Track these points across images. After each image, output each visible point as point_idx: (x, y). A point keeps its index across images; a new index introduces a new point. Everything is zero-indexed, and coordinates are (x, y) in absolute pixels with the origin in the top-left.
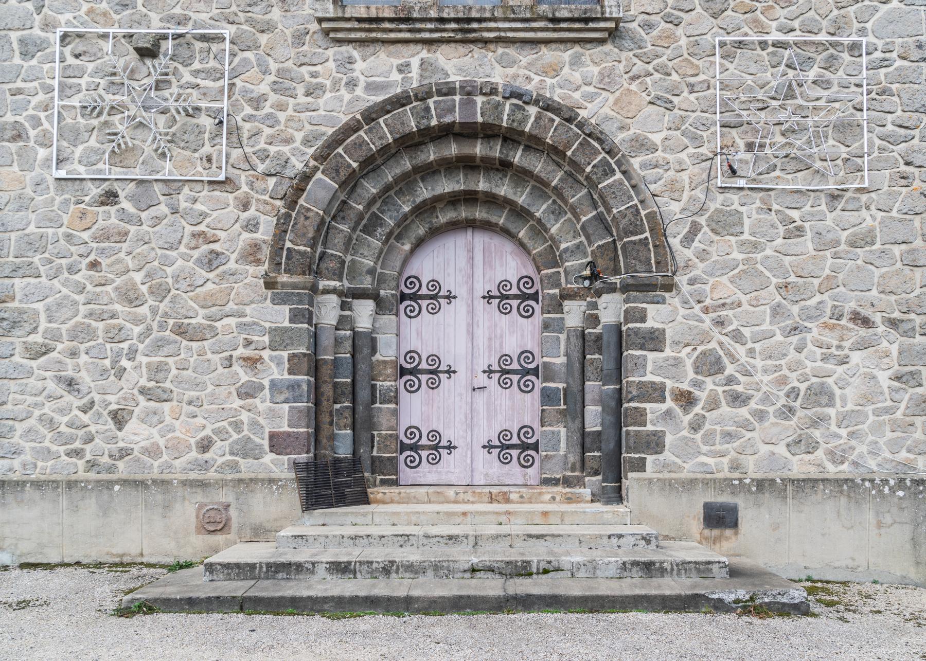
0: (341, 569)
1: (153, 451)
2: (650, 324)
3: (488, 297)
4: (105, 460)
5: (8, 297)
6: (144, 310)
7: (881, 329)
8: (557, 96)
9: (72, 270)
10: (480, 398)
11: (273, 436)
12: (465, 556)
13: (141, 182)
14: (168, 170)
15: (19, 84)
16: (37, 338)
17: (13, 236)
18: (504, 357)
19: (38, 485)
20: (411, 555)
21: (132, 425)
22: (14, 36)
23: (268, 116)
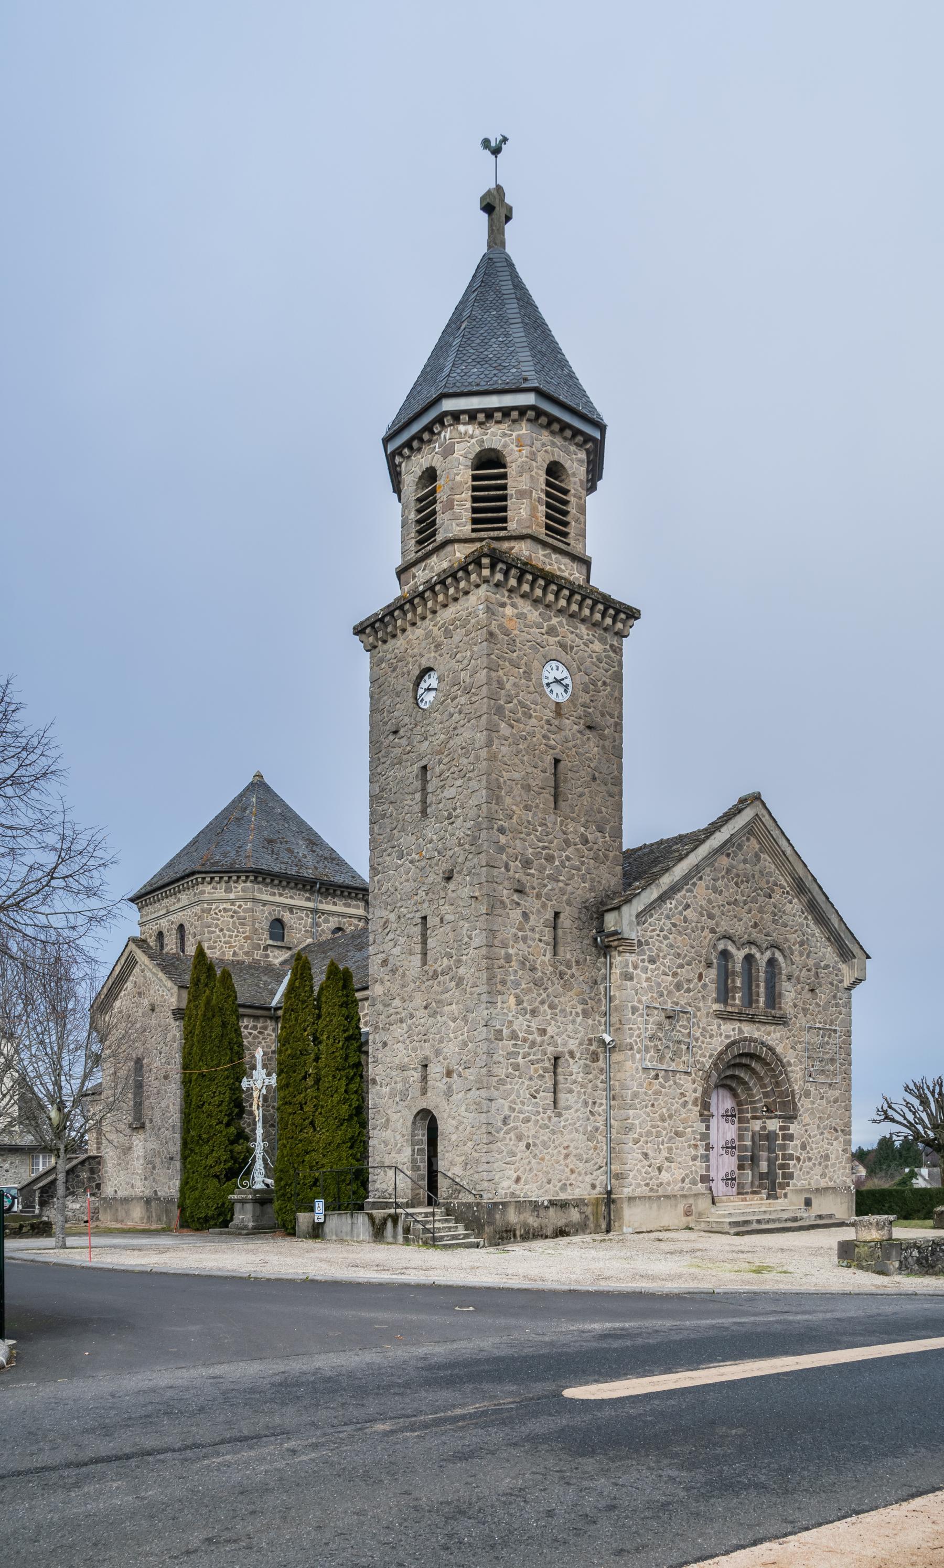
0: (759, 1221)
1: (669, 1184)
2: (791, 1131)
3: (723, 1116)
4: (655, 1187)
5: (844, 1151)
6: (666, 1124)
7: (840, 1133)
8: (770, 1043)
9: (646, 1107)
10: (720, 1159)
11: (701, 1176)
12: (785, 1216)
13: (666, 1071)
14: (673, 1066)
15: (631, 1026)
16: (636, 1136)
17: (630, 1092)
18: (727, 1142)
19: (640, 1198)
20: (767, 1217)
21: (663, 1172)
22: (630, 1004)
23: (700, 1046)
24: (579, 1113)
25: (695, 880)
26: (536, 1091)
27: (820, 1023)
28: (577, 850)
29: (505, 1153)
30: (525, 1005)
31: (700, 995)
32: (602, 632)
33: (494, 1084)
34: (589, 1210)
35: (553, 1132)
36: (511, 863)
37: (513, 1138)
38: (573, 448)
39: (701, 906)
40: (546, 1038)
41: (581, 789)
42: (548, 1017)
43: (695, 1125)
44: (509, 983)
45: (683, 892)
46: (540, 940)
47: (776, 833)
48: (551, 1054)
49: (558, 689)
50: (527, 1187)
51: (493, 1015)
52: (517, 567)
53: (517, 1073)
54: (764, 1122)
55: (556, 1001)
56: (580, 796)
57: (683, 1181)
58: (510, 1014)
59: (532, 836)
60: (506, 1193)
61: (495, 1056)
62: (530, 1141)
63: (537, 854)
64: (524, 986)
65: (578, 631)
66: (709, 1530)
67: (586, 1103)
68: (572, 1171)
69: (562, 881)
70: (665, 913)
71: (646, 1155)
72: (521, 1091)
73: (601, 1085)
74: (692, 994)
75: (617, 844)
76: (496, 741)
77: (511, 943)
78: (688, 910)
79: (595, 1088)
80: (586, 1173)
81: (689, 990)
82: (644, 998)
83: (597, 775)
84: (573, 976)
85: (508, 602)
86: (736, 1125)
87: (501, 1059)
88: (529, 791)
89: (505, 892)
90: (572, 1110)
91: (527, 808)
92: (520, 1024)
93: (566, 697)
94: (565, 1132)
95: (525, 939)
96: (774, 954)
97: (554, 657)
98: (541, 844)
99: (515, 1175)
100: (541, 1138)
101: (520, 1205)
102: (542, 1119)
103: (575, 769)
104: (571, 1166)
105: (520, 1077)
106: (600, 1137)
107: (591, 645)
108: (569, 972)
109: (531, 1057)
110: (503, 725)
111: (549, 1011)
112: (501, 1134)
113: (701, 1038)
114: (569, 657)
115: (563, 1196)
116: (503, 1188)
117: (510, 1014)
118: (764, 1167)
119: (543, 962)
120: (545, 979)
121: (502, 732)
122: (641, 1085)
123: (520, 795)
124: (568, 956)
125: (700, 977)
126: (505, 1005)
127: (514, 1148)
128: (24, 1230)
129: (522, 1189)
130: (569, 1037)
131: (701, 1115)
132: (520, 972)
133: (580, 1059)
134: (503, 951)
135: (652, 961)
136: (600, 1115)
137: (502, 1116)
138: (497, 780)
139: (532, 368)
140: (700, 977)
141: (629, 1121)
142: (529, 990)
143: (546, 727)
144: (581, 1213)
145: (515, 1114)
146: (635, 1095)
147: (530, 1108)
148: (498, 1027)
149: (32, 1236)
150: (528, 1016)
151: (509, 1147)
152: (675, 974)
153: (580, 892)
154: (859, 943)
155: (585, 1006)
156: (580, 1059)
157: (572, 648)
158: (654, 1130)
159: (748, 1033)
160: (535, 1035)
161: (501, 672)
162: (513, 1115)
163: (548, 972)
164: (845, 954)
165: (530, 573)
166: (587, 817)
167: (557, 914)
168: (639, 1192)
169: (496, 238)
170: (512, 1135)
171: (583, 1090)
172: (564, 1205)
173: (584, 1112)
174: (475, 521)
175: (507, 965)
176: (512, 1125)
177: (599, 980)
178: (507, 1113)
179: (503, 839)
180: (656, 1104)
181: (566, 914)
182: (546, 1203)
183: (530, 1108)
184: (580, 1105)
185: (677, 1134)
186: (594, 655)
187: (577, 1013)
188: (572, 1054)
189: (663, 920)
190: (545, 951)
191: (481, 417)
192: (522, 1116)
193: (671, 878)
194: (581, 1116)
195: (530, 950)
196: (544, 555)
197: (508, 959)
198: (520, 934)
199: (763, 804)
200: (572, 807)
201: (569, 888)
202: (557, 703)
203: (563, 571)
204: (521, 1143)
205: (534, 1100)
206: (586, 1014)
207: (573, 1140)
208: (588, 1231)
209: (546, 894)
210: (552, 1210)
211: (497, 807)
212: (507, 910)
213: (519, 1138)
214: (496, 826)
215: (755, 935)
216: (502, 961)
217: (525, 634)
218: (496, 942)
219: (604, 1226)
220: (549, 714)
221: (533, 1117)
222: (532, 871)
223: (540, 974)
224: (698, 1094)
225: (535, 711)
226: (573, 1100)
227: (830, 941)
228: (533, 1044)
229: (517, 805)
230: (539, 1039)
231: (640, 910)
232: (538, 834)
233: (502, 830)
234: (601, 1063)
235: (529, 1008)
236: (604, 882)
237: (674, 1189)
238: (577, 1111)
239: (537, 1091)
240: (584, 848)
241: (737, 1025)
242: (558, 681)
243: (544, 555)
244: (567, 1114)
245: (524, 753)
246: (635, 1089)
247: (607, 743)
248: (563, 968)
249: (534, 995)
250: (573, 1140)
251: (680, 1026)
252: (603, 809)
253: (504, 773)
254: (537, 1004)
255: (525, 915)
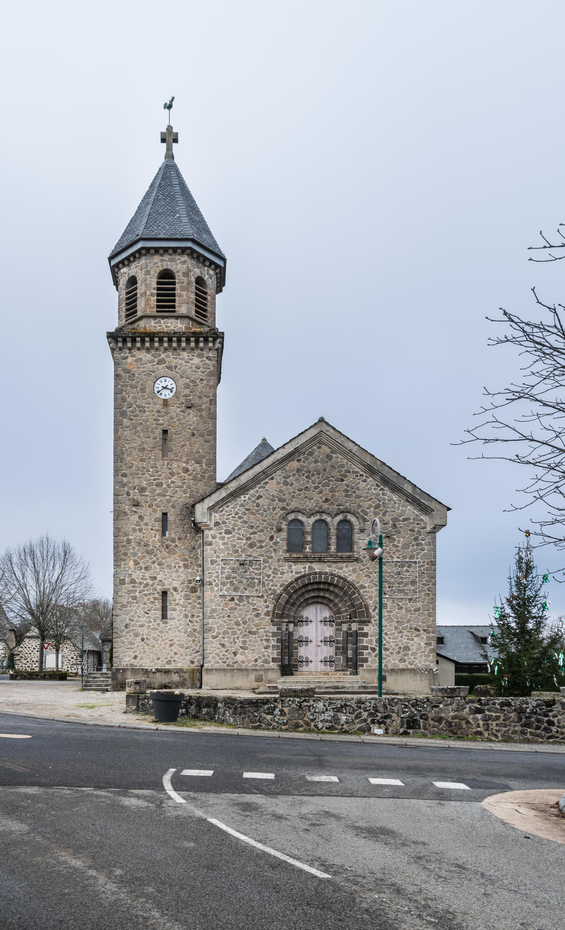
2: (365, 631)
3: (321, 621)
4: (231, 664)
6: (241, 627)
7: (422, 632)
9: (223, 617)
10: (319, 649)
11: (273, 658)
14: (247, 593)
15: (210, 571)
16: (215, 634)
17: (209, 609)
18: (325, 638)
19: (216, 670)
21: (238, 655)
23: (272, 580)
24: (181, 622)
25: (267, 480)
26: (148, 610)
27: (398, 558)
28: (180, 477)
29: (126, 643)
30: (141, 565)
31: (271, 549)
32: (200, 351)
33: (119, 607)
34: (187, 676)
35: (161, 632)
36: (131, 491)
37: (132, 635)
38: (177, 257)
39: (273, 496)
40: (156, 581)
41: (183, 443)
42: (158, 570)
43: (266, 627)
44: (129, 554)
45: (257, 489)
46: (152, 529)
47: (340, 440)
48: (160, 590)
49: (166, 392)
50: (142, 661)
51: (118, 572)
52: (129, 337)
53: (135, 601)
54: (350, 625)
55: (164, 561)
56: (183, 446)
57: (256, 660)
58: (130, 571)
59: (146, 475)
60: (127, 664)
61: (119, 593)
62: (144, 637)
63: (149, 484)
64: (140, 555)
65: (181, 356)
66: (445, 906)
67: (186, 616)
68: (175, 654)
69: (169, 495)
70: (240, 503)
71: (223, 645)
72: (138, 611)
73: (198, 606)
74: (264, 549)
75: (212, 468)
76: (120, 430)
77: (131, 533)
78: (261, 499)
79: (194, 607)
80: (186, 655)
81: (261, 547)
82: (221, 555)
83: (195, 432)
84: (176, 546)
85: (129, 355)
86: (334, 627)
87: (124, 594)
88: (144, 451)
89: (127, 507)
90: (176, 620)
91: (142, 460)
92: (137, 575)
93: (172, 395)
94: (170, 632)
95: (140, 530)
96: (346, 517)
97: (162, 375)
98: (152, 478)
99: (134, 655)
100: (152, 635)
101: (135, 671)
102: (153, 625)
103: (178, 432)
104: (175, 650)
105: (136, 603)
106: (197, 635)
107: (191, 361)
108: (174, 544)
109: (146, 592)
110: (125, 420)
111: (158, 567)
112: (124, 633)
113: (272, 575)
114: (174, 372)
115: (168, 667)
116: (125, 661)
117: (130, 571)
118: (350, 654)
119: (154, 541)
120: (155, 550)
121: (125, 424)
122: (219, 605)
123: (137, 455)
124: (173, 536)
125: (272, 538)
126: (127, 566)
127: (133, 641)
128: (47, 677)
129: (139, 662)
130: (173, 580)
131: (272, 621)
132: (137, 548)
133: (181, 592)
134: (125, 538)
135: (228, 532)
136: (197, 622)
137: (125, 624)
138: (121, 449)
139: (185, 213)
140: (272, 538)
141: (209, 626)
142: (144, 557)
143: (156, 414)
144: (180, 677)
145: (134, 622)
146: (214, 611)
147: (144, 619)
148: (122, 578)
149: (50, 680)
150: (143, 571)
151: (129, 640)
152: (248, 539)
153: (182, 499)
154: (437, 500)
155: (186, 562)
156: (181, 592)
157: (176, 367)
158: (230, 631)
159: (318, 569)
160: (149, 580)
161: (124, 393)
162: (132, 623)
163: (157, 546)
164: (426, 510)
165: (139, 337)
166: (188, 457)
167: (165, 514)
168: (217, 666)
169: (170, 156)
170: (131, 634)
171: (184, 609)
172: (167, 672)
173: (184, 621)
174: (158, 307)
175: (128, 545)
176: (131, 628)
177: (197, 547)
178: (128, 622)
179: (125, 480)
180: (231, 615)
181: (171, 513)
182: (154, 670)
183: (144, 619)
184: (181, 617)
185: (250, 632)
186: (193, 366)
187: (180, 567)
188: (175, 589)
189: (238, 508)
190: (155, 535)
191: (126, 262)
192: (138, 624)
193: (238, 483)
194: (183, 623)
195: (144, 535)
196: (154, 323)
197: (129, 542)
198: (137, 528)
199: (327, 424)
200: (176, 455)
201: (173, 499)
202: (164, 400)
203: (170, 327)
204: (137, 638)
205: (146, 615)
206: (186, 566)
207: (176, 637)
208: (186, 687)
209: (156, 504)
210: (158, 674)
211: (121, 464)
212: (128, 516)
213: (136, 635)
214: (120, 474)
215: (325, 506)
216: (125, 543)
217: (141, 369)
218: (120, 534)
219: (198, 685)
220: (159, 407)
221: (146, 624)
222: (147, 493)
223: (151, 547)
224: (270, 609)
225: (148, 408)
226: (176, 614)
227: (409, 502)
228: (147, 585)
229: (135, 460)
230: (151, 582)
231: (211, 505)
232: (150, 473)
233: (124, 475)
234: (198, 594)
235: (143, 566)
236: (201, 491)
237: (250, 665)
238: (179, 620)
239: (149, 610)
240: (185, 475)
241: (307, 565)
242: (165, 388)
243: (154, 323)
244: (170, 622)
245: (140, 431)
246: (213, 607)
247: (204, 413)
248: (169, 543)
249: (148, 559)
250: (176, 637)
251: (253, 569)
252: (201, 450)
253: (126, 445)
254: (149, 563)
255: (141, 518)
